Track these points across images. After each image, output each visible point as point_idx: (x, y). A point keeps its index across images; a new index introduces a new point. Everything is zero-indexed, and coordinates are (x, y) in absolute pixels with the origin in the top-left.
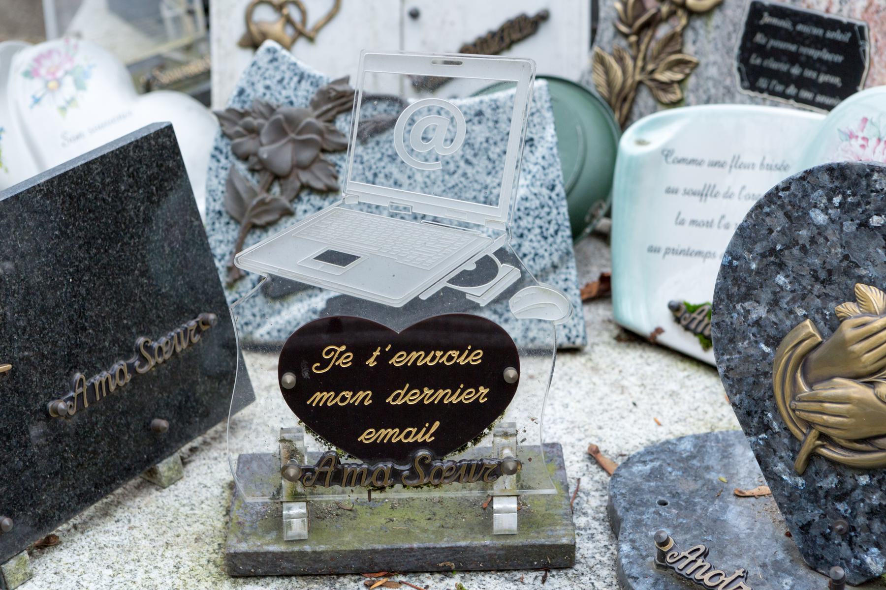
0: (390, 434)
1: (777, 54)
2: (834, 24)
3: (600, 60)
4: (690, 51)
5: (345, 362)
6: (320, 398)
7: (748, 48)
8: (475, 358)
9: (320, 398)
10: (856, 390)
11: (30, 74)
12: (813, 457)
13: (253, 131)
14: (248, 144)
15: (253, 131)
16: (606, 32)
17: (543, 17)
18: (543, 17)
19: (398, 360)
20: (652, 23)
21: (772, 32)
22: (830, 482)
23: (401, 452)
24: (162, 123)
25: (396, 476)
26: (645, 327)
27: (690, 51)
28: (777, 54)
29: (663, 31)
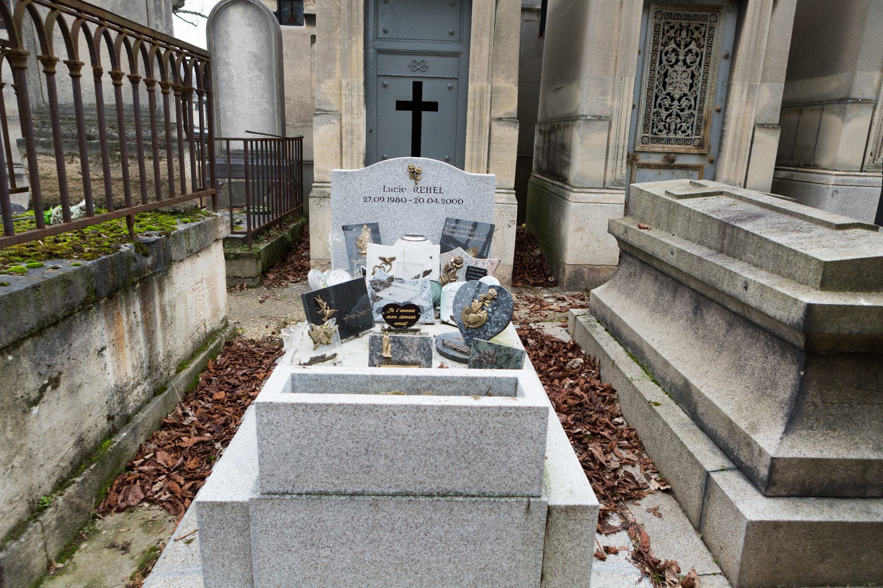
0: (399, 324)
1: (472, 275)
2: (482, 269)
3: (440, 277)
4: (457, 275)
5: (393, 311)
6: (388, 317)
7: (467, 274)
8: (414, 311)
9: (388, 317)
10: (473, 315)
11: (334, 275)
12: (468, 327)
13: (376, 284)
14: (375, 286)
15: (376, 284)
16: (442, 272)
17: (431, 271)
18: (431, 271)
19: (402, 311)
20: (450, 270)
21: (471, 271)
22: (470, 331)
23: (401, 327)
24: (287, 383)
25: (400, 331)
26: (446, 321)
27: (457, 275)
28: (472, 275)
29: (452, 271)
